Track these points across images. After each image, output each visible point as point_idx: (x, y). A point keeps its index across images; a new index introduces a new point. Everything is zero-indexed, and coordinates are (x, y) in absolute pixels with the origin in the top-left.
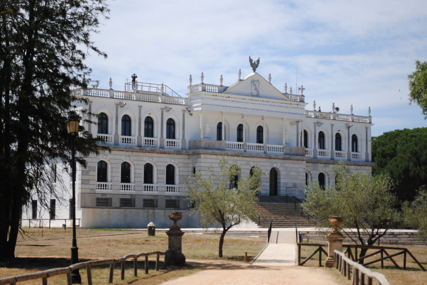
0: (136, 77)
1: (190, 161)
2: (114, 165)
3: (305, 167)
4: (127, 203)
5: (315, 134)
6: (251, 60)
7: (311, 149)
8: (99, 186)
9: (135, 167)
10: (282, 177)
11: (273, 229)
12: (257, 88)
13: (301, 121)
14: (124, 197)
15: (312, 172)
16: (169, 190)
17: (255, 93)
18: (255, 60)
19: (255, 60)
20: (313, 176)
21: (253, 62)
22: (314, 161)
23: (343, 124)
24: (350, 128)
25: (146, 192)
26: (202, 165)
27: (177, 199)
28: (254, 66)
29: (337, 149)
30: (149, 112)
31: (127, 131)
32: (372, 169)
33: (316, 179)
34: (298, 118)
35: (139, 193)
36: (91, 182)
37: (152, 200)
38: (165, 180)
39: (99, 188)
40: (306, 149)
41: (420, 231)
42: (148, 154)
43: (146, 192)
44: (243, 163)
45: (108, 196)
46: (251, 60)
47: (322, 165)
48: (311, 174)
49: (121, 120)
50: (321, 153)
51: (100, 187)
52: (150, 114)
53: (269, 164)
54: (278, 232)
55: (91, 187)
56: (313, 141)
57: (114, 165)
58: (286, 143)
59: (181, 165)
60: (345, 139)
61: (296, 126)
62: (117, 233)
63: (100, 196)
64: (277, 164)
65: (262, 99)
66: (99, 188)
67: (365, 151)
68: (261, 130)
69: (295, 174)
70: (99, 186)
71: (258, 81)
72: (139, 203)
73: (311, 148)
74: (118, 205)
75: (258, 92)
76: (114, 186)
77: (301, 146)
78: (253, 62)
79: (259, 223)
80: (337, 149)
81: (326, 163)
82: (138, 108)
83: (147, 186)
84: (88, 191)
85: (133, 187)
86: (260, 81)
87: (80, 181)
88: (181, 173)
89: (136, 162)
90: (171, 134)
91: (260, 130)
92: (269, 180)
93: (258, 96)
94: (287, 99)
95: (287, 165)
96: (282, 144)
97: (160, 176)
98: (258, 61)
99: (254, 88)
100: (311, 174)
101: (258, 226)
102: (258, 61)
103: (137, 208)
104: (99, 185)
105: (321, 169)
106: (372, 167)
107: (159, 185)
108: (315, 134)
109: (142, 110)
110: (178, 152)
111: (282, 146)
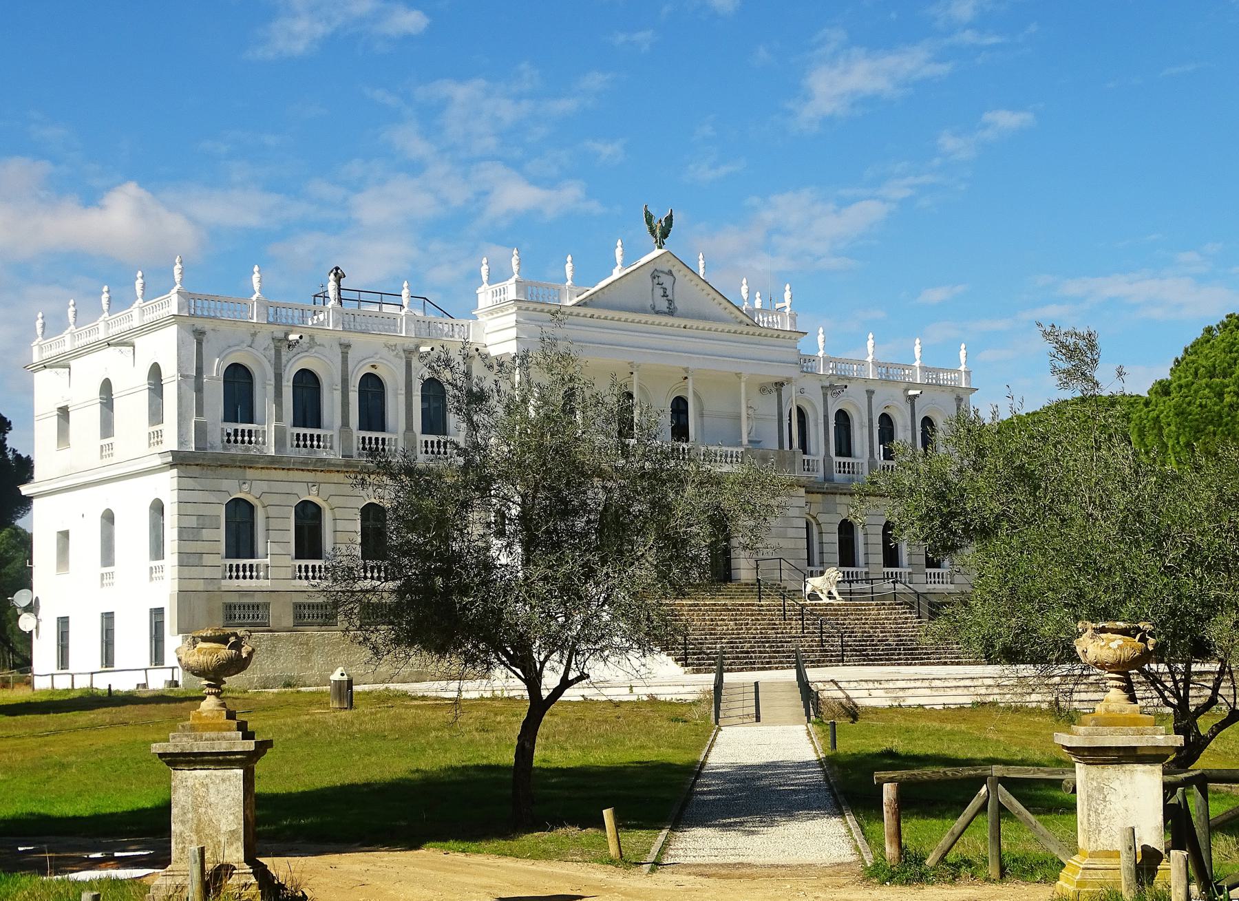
2: (272, 511)
3: (802, 502)
5: (826, 417)
6: (649, 219)
7: (860, 461)
8: (231, 571)
9: (334, 514)
11: (728, 677)
13: (789, 380)
17: (663, 304)
18: (659, 216)
22: (825, 489)
23: (898, 392)
29: (839, 453)
30: (372, 361)
31: (844, 450)
34: (779, 373)
38: (222, 547)
39: (231, 577)
40: (806, 457)
45: (258, 599)
48: (818, 524)
49: (291, 384)
51: (234, 574)
52: (373, 366)
54: (756, 683)
55: (208, 573)
56: (821, 439)
57: (272, 511)
58: (750, 442)
60: (396, 395)
61: (775, 394)
62: (682, 697)
63: (234, 599)
65: (683, 322)
66: (231, 577)
68: (682, 407)
70: (231, 571)
71: (670, 273)
73: (818, 454)
74: (289, 621)
75: (670, 302)
77: (791, 447)
79: (686, 659)
80: (839, 453)
82: (338, 350)
83: (238, 566)
84: (201, 586)
85: (262, 568)
86: (674, 271)
87: (176, 556)
89: (336, 501)
91: (679, 407)
93: (671, 312)
94: (749, 321)
96: (740, 444)
98: (669, 219)
100: (818, 524)
101: (682, 670)
104: (231, 566)
108: (826, 417)
109: (351, 354)
111: (741, 450)
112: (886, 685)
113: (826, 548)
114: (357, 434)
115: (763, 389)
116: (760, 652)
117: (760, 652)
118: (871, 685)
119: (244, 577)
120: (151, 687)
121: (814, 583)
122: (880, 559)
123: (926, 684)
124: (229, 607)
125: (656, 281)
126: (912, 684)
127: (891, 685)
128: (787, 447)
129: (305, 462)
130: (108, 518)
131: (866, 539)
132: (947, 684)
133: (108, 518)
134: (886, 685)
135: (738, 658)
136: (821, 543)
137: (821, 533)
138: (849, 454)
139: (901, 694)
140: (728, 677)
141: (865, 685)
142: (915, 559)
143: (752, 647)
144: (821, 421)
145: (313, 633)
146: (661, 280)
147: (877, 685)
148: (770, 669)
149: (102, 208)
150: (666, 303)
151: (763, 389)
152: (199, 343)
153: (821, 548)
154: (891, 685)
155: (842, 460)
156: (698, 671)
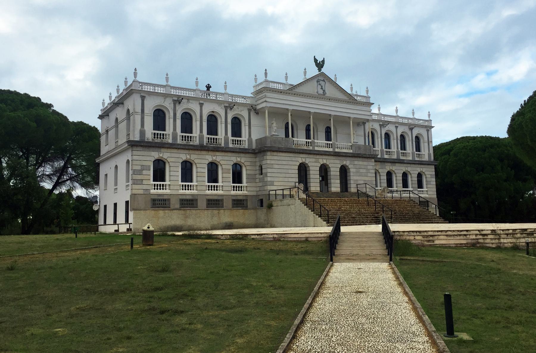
0: (211, 87)
1: (257, 159)
4: (239, 203)
6: (316, 60)
10: (351, 174)
11: (343, 229)
12: (323, 87)
14: (184, 197)
15: (380, 171)
16: (210, 188)
18: (320, 60)
19: (320, 60)
20: (381, 174)
21: (318, 62)
24: (413, 130)
25: (210, 192)
26: (268, 162)
27: (244, 198)
28: (320, 66)
32: (435, 168)
33: (384, 178)
35: (174, 192)
36: (145, 182)
37: (217, 200)
41: (266, 188)
42: (211, 153)
43: (210, 192)
44: (311, 160)
46: (316, 60)
47: (390, 164)
50: (387, 153)
53: (338, 161)
55: (145, 187)
59: (248, 164)
63: (156, 197)
64: (347, 162)
67: (426, 154)
68: (329, 130)
69: (364, 171)
72: (174, 203)
73: (410, 150)
74: (178, 206)
75: (324, 91)
76: (173, 185)
78: (318, 62)
81: (394, 162)
88: (249, 172)
90: (237, 131)
92: (339, 177)
95: (356, 162)
97: (225, 175)
99: (320, 87)
102: (323, 61)
103: (200, 208)
105: (389, 167)
106: (435, 166)
107: (225, 184)
110: (244, 151)
112: (423, 234)
113: (382, 181)
114: (231, 138)
118: (415, 234)
119: (160, 189)
120: (120, 231)
122: (401, 185)
123: (444, 233)
124: (154, 200)
126: (437, 233)
127: (425, 234)
128: (367, 144)
129: (184, 145)
130: (116, 167)
131: (380, 178)
132: (454, 233)
133: (116, 167)
134: (423, 234)
139: (431, 238)
140: (343, 229)
141: (412, 234)
142: (414, 186)
146: (320, 83)
147: (418, 234)
149: (322, 78)
150: (322, 91)
152: (397, 129)
153: (380, 178)
154: (425, 234)
155: (403, 151)
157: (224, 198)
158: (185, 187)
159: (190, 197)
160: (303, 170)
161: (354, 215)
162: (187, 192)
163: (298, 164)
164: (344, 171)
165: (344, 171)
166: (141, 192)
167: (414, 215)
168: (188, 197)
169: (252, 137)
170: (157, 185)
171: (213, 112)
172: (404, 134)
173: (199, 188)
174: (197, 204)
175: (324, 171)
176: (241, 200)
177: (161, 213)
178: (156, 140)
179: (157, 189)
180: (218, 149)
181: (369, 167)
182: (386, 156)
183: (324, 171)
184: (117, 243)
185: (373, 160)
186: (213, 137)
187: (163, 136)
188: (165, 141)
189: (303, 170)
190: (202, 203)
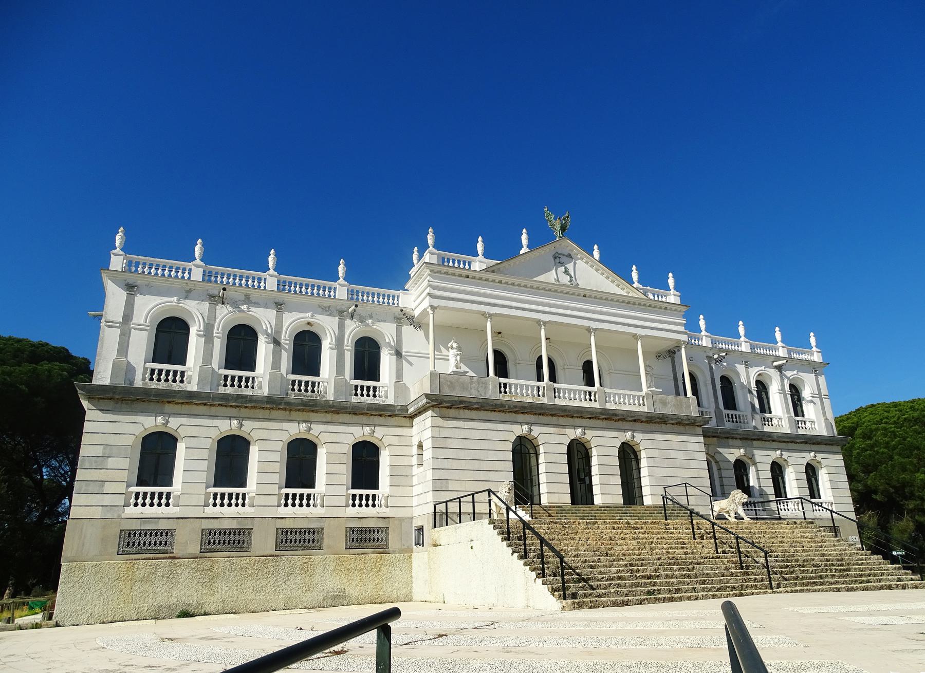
14: (215, 525)
27: (381, 524)
45: (163, 525)
55: (107, 500)
72: (187, 541)
79: (564, 589)
100: (717, 462)
113: (725, 482)
115: (659, 356)
116: (667, 576)
117: (667, 576)
121: (720, 505)
125: (558, 260)
135: (637, 585)
136: (721, 477)
137: (719, 469)
138: (734, 408)
143: (656, 570)
144: (709, 381)
145: (221, 560)
148: (681, 599)
151: (659, 356)
153: (720, 473)
155: (731, 412)
156: (580, 606)
157: (326, 524)
158: (220, 500)
159: (234, 525)
160: (524, 455)
161: (650, 569)
162: (227, 511)
163: (513, 439)
164: (628, 458)
165: (628, 458)
166: (98, 513)
167: (829, 564)
168: (227, 525)
169: (407, 380)
170: (361, 496)
171: (309, 324)
172: (760, 378)
173: (120, 501)
174: (249, 543)
175: (578, 458)
176: (370, 530)
177: (142, 566)
178: (154, 385)
179: (222, 505)
180: (314, 408)
181: (691, 447)
182: (728, 426)
183: (578, 458)
184: (851, 576)
185: (699, 430)
186: (304, 378)
187: (313, 386)
188: (316, 397)
189: (524, 455)
190: (335, 538)
